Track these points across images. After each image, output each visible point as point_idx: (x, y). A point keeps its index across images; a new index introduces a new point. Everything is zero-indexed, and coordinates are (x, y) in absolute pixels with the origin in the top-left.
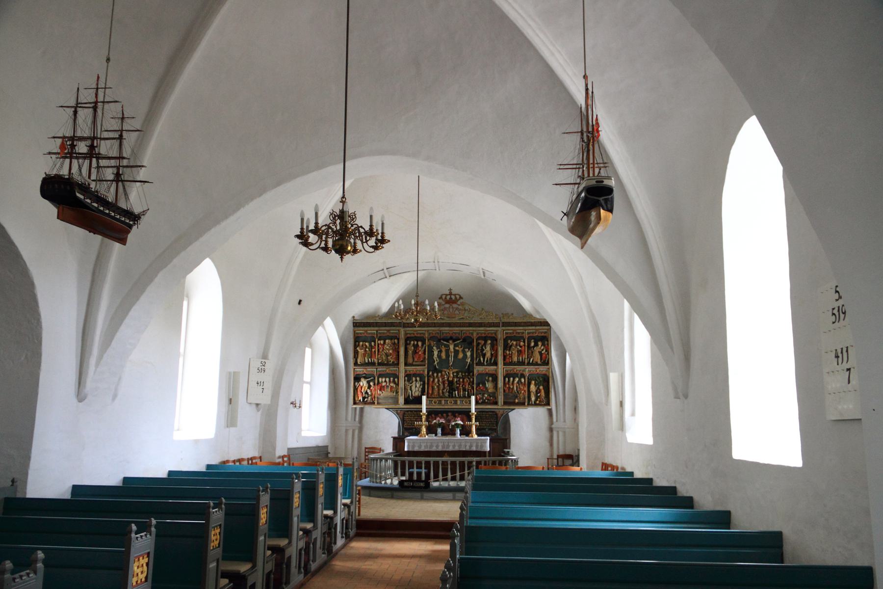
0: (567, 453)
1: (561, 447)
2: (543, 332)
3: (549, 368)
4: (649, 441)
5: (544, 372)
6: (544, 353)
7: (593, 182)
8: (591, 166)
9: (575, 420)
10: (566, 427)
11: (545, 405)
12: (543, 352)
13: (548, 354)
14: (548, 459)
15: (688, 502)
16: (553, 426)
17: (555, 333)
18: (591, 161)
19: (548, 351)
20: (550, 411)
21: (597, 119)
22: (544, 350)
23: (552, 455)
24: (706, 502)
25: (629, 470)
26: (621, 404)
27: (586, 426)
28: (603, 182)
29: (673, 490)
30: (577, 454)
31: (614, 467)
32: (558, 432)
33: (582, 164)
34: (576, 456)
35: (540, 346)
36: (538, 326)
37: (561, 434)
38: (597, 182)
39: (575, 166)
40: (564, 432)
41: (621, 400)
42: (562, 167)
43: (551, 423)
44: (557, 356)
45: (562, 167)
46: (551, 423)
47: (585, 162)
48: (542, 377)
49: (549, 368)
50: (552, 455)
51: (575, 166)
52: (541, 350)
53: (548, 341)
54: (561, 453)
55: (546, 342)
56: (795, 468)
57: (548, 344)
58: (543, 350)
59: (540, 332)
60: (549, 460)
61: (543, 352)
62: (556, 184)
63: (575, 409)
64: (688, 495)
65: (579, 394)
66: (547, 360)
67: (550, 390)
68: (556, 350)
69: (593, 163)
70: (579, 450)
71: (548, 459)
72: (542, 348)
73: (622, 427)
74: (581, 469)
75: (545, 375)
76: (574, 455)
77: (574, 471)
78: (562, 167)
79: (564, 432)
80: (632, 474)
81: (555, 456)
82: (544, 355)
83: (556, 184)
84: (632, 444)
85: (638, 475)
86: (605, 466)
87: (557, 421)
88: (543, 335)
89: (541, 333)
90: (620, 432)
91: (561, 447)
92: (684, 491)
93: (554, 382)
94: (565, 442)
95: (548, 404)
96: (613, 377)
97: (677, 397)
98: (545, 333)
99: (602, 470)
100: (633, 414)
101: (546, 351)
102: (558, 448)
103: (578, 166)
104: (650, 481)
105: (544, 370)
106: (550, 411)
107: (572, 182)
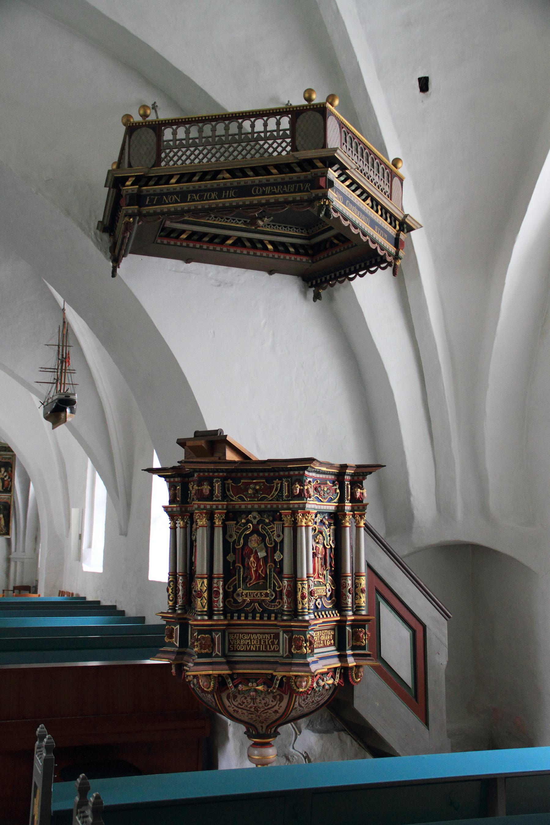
0: (25, 584)
1: (18, 579)
2: (7, 458)
3: (11, 496)
4: (100, 570)
5: (5, 500)
6: (7, 480)
7: (63, 396)
8: (64, 371)
9: (35, 550)
10: (25, 557)
11: (4, 534)
12: (5, 479)
13: (11, 481)
14: (3, 591)
15: (123, 613)
16: (11, 556)
17: (19, 460)
18: (64, 368)
19: (11, 478)
20: (9, 541)
21: (69, 354)
22: (7, 477)
23: (8, 586)
24: (131, 612)
25: (82, 595)
26: (80, 537)
27: (46, 557)
28: (69, 397)
29: (114, 607)
30: (35, 585)
31: (68, 594)
32: (16, 562)
33: (57, 369)
34: (34, 587)
35: (3, 472)
36: (3, 451)
37: (18, 564)
38: (65, 396)
39: (52, 370)
40: (23, 563)
41: (80, 533)
42: (42, 370)
43: (9, 552)
44: (21, 483)
45: (44, 370)
46: (9, 552)
47: (60, 368)
48: (3, 505)
49: (11, 496)
50: (8, 586)
51: (52, 370)
52: (3, 477)
53: (11, 467)
54: (18, 584)
55: (10, 469)
56: (160, 583)
57: (12, 471)
58: (6, 476)
59: (4, 458)
60: (5, 592)
61: (5, 479)
62: (37, 382)
63: (36, 539)
64: (122, 609)
65: (40, 520)
66: (9, 487)
67: (11, 518)
68: (19, 477)
69: (65, 370)
70: (37, 581)
71: (3, 591)
72: (5, 474)
73: (79, 557)
74: (39, 596)
75: (6, 503)
76: (32, 586)
77: (33, 597)
78: (42, 370)
79: (23, 563)
80: (85, 598)
81: (11, 588)
82: (6, 482)
83: (37, 382)
84: (87, 572)
85: (90, 598)
86: (62, 593)
87: (15, 551)
88: (7, 460)
89: (6, 458)
90: (78, 562)
91: (18, 579)
92: (120, 608)
93: (15, 513)
94: (22, 573)
95: (8, 533)
96: (74, 512)
97: (121, 534)
98: (9, 458)
99: (59, 596)
100: (90, 546)
101: (9, 478)
102: (15, 580)
103: (54, 370)
104: (99, 602)
105: (5, 498)
106: (9, 541)
107: (51, 382)
